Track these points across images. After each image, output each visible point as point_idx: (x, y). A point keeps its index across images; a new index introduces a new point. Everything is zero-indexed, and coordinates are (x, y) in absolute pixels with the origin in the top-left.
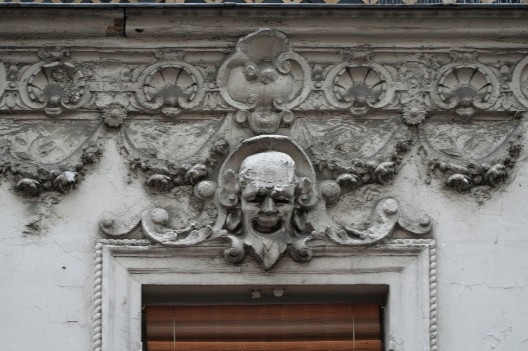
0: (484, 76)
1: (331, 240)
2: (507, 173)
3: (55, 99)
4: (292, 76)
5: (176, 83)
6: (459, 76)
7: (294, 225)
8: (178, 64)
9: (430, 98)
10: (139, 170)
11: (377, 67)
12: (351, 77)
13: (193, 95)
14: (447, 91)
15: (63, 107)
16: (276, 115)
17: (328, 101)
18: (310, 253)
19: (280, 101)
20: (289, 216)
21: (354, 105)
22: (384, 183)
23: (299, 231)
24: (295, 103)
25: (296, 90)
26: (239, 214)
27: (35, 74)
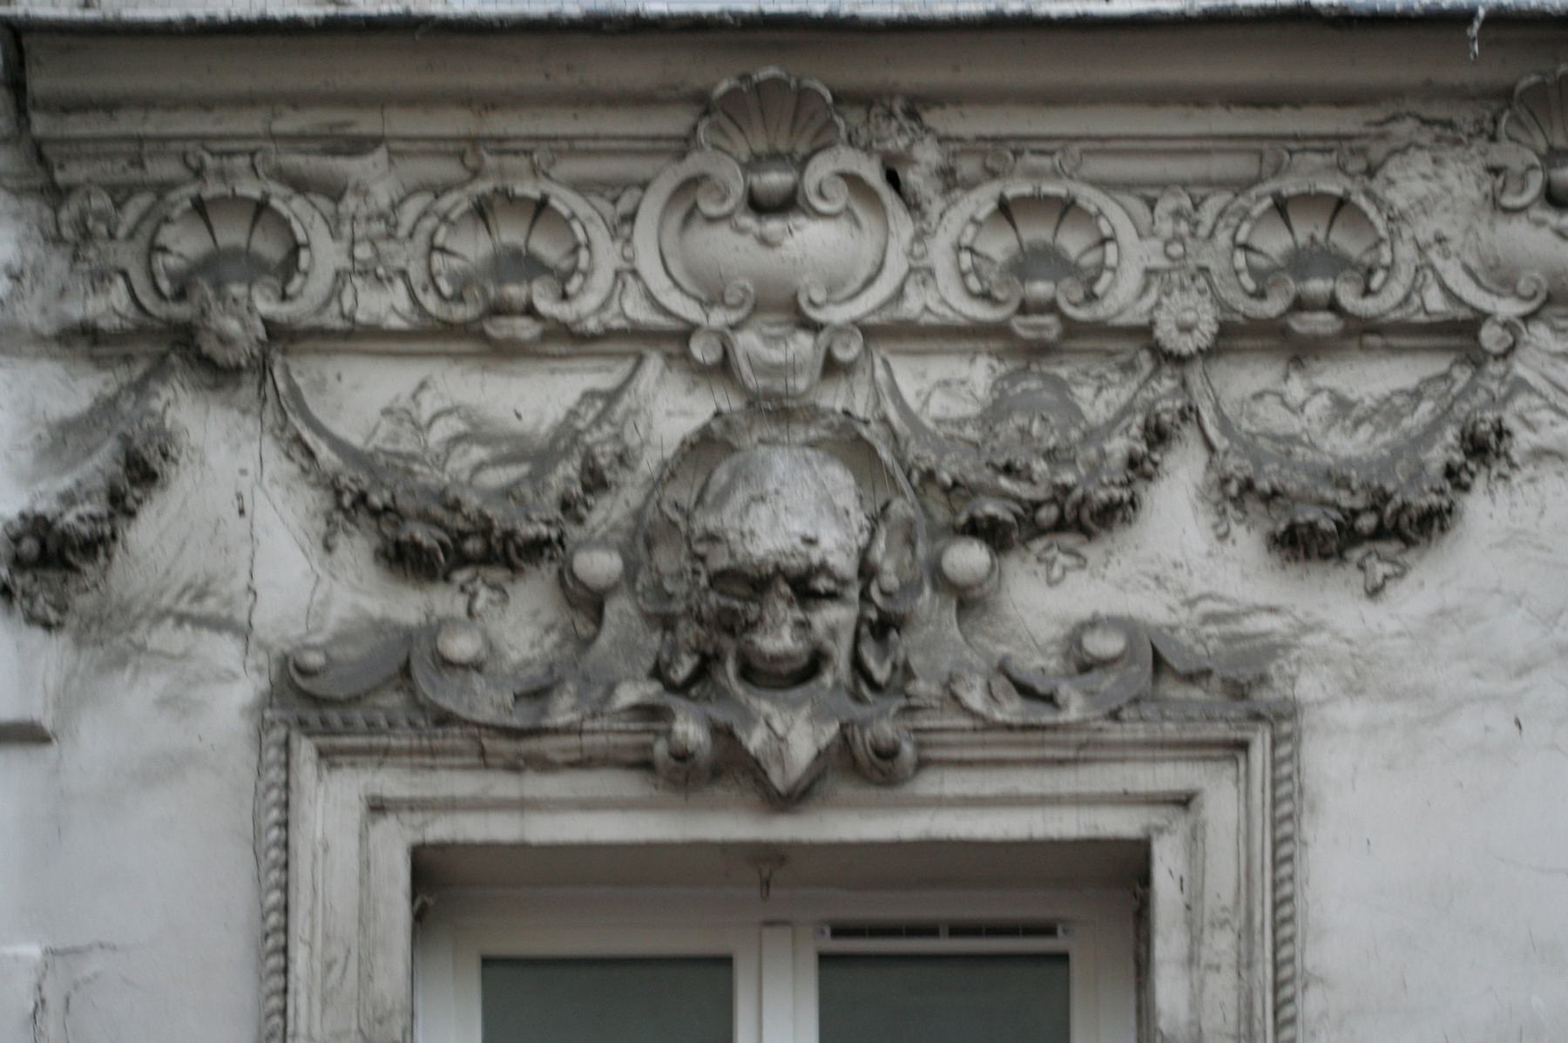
0: (565, 222)
2: (1452, 503)
3: (1040, 289)
5: (527, 241)
7: (857, 664)
8: (1333, 186)
10: (1252, 504)
12: (1014, 227)
15: (1063, 317)
17: (947, 299)
19: (818, 297)
20: (846, 640)
21: (1024, 309)
23: (875, 687)
27: (982, 215)
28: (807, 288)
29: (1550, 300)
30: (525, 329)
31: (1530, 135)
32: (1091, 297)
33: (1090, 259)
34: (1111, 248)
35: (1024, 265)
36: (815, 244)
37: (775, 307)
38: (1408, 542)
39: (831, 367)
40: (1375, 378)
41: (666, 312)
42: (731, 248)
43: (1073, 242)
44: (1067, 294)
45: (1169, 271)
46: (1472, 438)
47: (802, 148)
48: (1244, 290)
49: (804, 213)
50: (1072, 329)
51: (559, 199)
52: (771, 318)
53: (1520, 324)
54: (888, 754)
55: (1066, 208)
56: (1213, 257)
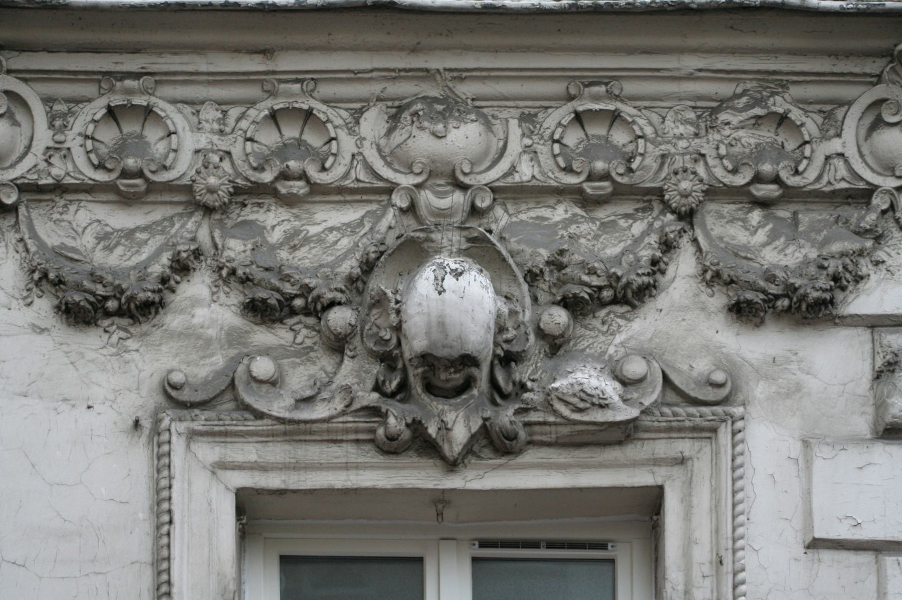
9: (706, 164)
11: (318, 106)
13: (172, 155)
15: (614, 182)
16: (443, 191)
18: (522, 434)
21: (590, 178)
22: (141, 319)
23: (505, 396)
26: (400, 366)
30: (298, 187)
40: (330, 217)
41: (379, 177)
44: (617, 169)
52: (442, 182)
55: (615, 117)
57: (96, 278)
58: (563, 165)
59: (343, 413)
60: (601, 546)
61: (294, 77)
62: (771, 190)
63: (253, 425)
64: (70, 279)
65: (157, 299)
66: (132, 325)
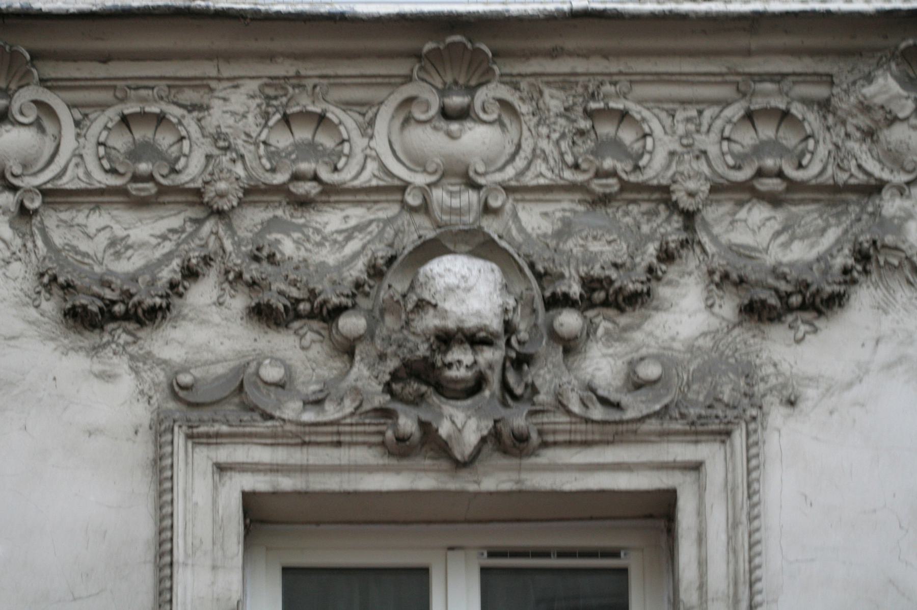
1: (569, 412)
3: (144, 167)
4: (502, 125)
6: (757, 123)
7: (505, 386)
14: (736, 148)
21: (136, 178)
23: (515, 398)
24: (510, 172)
25: (510, 149)
28: (11, 167)
29: (443, 176)
30: (308, 188)
31: (432, 77)
32: (637, 168)
33: (637, 146)
34: (649, 141)
35: (137, 153)
36: (477, 140)
37: (455, 175)
38: (820, 313)
39: (487, 210)
40: (332, 220)
42: (430, 140)
43: (164, 140)
44: (160, 171)
45: (683, 154)
46: (860, 252)
47: (473, 83)
48: (264, 167)
49: (474, 121)
50: (625, 186)
51: (333, 113)
52: (453, 181)
53: (905, 186)
54: (521, 439)
56: (709, 143)
57: (106, 284)
58: (107, 166)
59: (352, 414)
60: (615, 554)
61: (674, 78)
62: (773, 184)
63: (263, 427)
64: (753, 277)
65: (350, 304)
66: (138, 329)
